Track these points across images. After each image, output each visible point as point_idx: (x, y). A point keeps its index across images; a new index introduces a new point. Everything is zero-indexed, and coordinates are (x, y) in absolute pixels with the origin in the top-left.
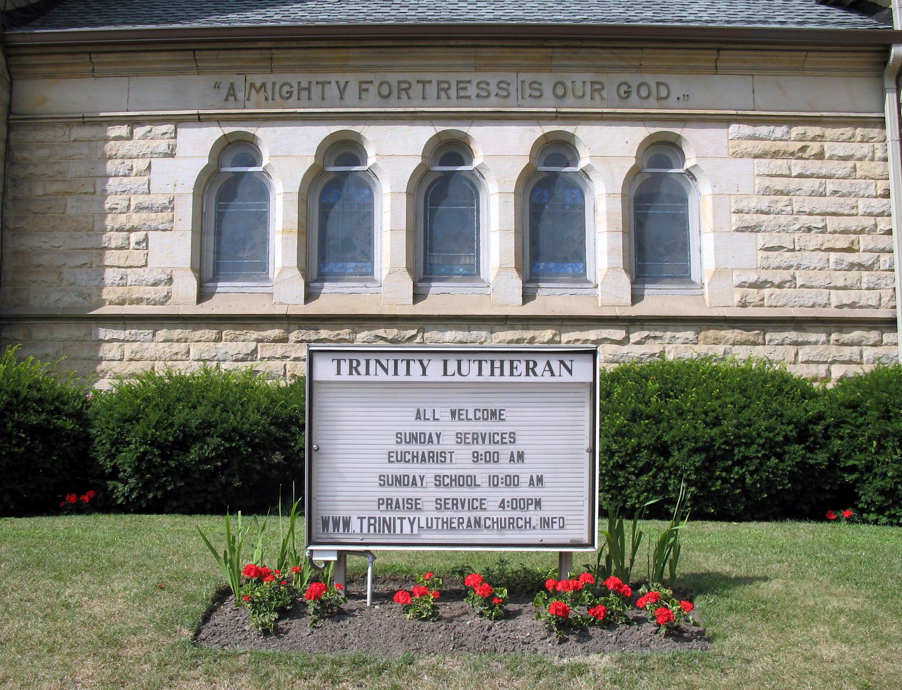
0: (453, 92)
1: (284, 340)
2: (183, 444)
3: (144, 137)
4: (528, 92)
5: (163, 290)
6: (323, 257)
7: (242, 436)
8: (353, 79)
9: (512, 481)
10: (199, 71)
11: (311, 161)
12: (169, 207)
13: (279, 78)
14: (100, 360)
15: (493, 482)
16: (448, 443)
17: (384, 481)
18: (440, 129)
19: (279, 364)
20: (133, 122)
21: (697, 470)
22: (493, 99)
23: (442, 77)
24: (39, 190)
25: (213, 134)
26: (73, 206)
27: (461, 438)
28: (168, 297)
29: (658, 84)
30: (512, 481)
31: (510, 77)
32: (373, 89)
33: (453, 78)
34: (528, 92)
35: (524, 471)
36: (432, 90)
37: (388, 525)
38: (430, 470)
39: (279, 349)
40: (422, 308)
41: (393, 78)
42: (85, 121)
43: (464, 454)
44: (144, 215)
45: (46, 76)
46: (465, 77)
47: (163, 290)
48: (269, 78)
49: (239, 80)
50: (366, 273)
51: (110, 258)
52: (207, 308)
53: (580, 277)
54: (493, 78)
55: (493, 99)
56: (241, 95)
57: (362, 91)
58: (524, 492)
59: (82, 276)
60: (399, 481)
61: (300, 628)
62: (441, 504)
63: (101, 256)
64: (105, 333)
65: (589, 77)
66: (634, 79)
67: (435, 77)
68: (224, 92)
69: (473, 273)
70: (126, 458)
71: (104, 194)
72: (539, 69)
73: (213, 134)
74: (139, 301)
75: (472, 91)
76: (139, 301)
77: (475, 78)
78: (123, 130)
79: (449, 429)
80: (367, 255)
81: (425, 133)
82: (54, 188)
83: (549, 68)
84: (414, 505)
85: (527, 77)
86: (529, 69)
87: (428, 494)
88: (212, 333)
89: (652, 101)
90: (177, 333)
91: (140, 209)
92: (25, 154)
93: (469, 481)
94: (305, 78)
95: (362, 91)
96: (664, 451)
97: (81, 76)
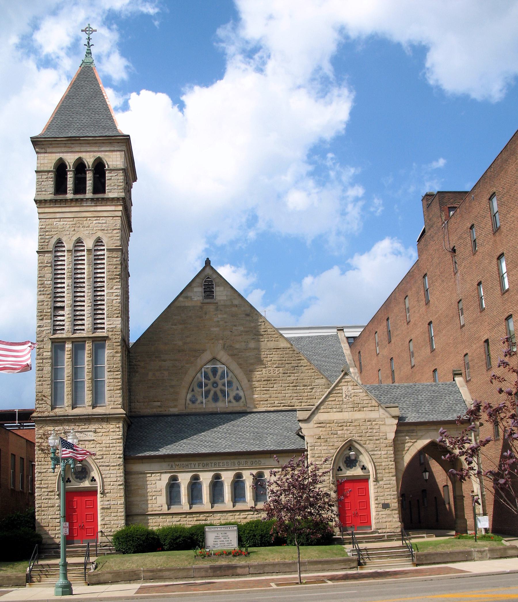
0: (217, 465)
1: (186, 517)
2: (178, 538)
3: (154, 476)
4: (232, 464)
5: (160, 508)
6: (192, 499)
7: (186, 537)
8: (197, 463)
9: (228, 541)
10: (165, 462)
11: (189, 480)
12: (161, 491)
13: (182, 463)
14: (148, 523)
15: (226, 541)
16: (221, 537)
17: (214, 542)
18: (215, 473)
19: (185, 522)
20: (152, 473)
21: (260, 539)
22: (225, 466)
23: (214, 462)
24: (133, 488)
25: (169, 475)
26: (140, 492)
27: (222, 536)
28: (162, 509)
29: (259, 461)
30: (228, 541)
31: (229, 461)
32: (201, 465)
33: (217, 462)
34: (232, 464)
35: (229, 540)
36: (213, 465)
37: (215, 546)
38: (219, 540)
39: (185, 519)
40: (213, 510)
41: (205, 462)
42: (141, 473)
43: (222, 538)
44: (156, 493)
45: (132, 463)
46: (219, 461)
47: (160, 508)
48: (179, 463)
49: (173, 464)
50: (201, 503)
51: (149, 502)
52: (170, 512)
53: (245, 501)
54: (225, 461)
55: (225, 466)
56: (174, 467)
57: (199, 465)
58: (229, 542)
59: (144, 506)
60: (215, 541)
61: (206, 558)
62: (220, 544)
63: (148, 502)
64: (149, 518)
65: (245, 460)
66: (254, 460)
67: (213, 462)
68: (170, 466)
69: (223, 501)
70: (167, 542)
71: (147, 489)
72: (234, 459)
73: (169, 475)
74: (156, 511)
75: (221, 464)
76: (156, 511)
77: (221, 461)
78: (150, 475)
79: (221, 535)
80: (201, 498)
81: (212, 474)
82: (136, 487)
83: (236, 459)
84: (217, 544)
85: (232, 461)
86: (232, 459)
87: (219, 543)
88: (171, 517)
89: (258, 465)
90: (164, 517)
91: (154, 491)
92: (129, 481)
93: (223, 541)
94: (187, 463)
95: (199, 465)
96: (255, 536)
97: (140, 463)
